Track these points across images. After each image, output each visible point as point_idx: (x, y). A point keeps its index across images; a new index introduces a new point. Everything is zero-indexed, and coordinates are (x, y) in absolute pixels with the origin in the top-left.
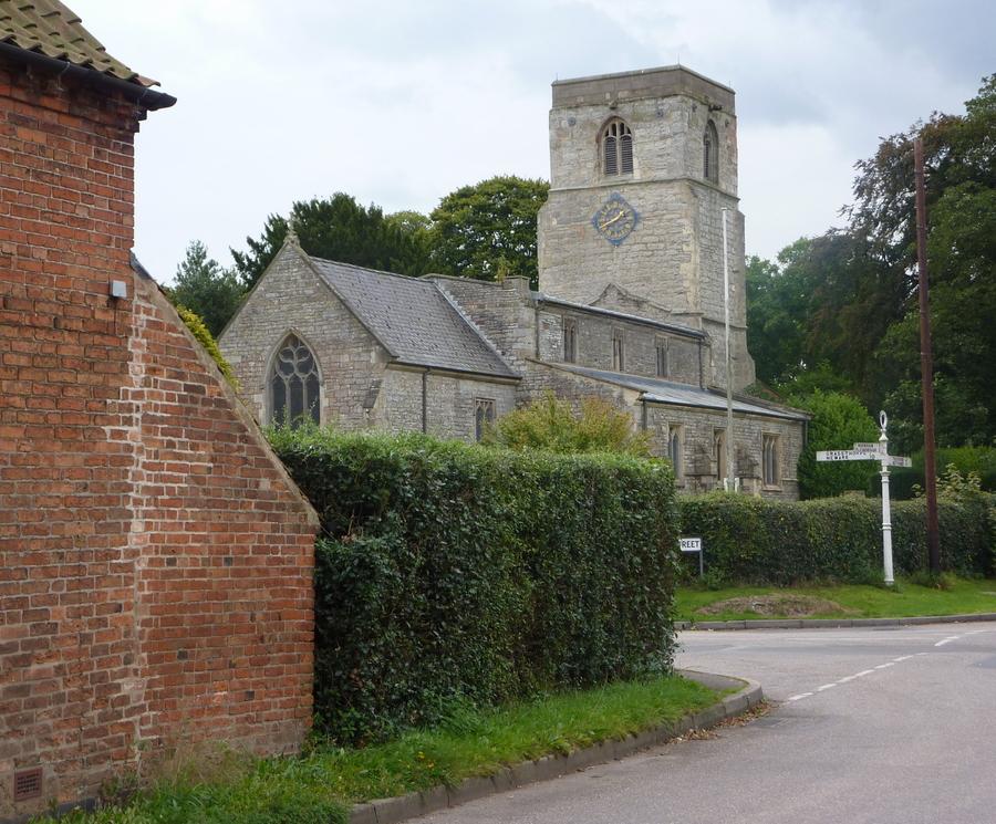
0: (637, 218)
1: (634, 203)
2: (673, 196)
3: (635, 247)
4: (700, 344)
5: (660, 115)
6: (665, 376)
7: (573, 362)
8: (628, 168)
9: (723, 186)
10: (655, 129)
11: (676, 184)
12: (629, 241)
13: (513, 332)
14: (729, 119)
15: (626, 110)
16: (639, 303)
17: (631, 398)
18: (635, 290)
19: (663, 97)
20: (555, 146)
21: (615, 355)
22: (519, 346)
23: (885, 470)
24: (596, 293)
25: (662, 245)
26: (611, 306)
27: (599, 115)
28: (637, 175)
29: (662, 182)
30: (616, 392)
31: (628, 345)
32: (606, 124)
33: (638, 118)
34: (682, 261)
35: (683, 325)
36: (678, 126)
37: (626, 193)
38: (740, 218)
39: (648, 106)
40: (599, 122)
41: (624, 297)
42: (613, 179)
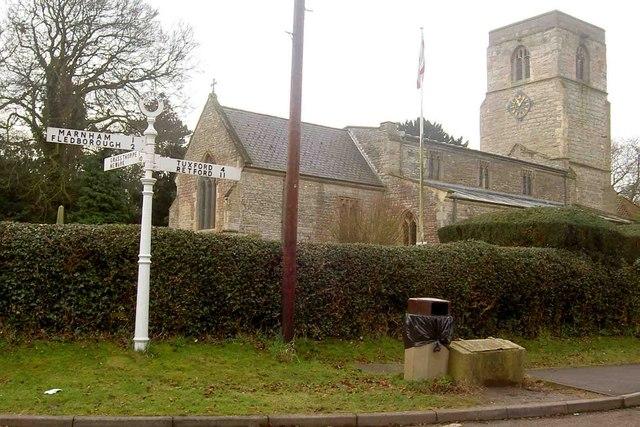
0: (532, 104)
1: (530, 94)
2: (551, 88)
3: (532, 121)
4: (565, 177)
5: (545, 41)
6: (530, 194)
7: (438, 179)
8: (528, 75)
9: (594, 85)
10: (542, 49)
11: (553, 81)
12: (528, 117)
13: (385, 157)
14: (599, 45)
15: (526, 41)
16: (532, 154)
17: (443, 195)
18: (530, 147)
19: (547, 30)
20: (490, 68)
21: (481, 179)
22: (386, 166)
23: (148, 176)
24: (509, 149)
25: (545, 119)
26: (517, 155)
27: (512, 46)
28: (532, 79)
29: (545, 80)
30: (435, 191)
31: (494, 172)
32: (516, 51)
33: (532, 45)
34: (555, 127)
35: (556, 165)
36: (555, 46)
37: (526, 90)
38: (608, 104)
39: (538, 37)
40: (512, 50)
41: (525, 151)
42: (521, 82)
